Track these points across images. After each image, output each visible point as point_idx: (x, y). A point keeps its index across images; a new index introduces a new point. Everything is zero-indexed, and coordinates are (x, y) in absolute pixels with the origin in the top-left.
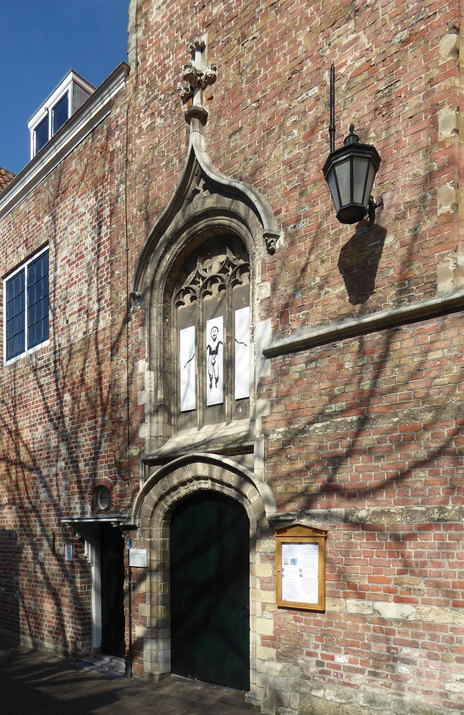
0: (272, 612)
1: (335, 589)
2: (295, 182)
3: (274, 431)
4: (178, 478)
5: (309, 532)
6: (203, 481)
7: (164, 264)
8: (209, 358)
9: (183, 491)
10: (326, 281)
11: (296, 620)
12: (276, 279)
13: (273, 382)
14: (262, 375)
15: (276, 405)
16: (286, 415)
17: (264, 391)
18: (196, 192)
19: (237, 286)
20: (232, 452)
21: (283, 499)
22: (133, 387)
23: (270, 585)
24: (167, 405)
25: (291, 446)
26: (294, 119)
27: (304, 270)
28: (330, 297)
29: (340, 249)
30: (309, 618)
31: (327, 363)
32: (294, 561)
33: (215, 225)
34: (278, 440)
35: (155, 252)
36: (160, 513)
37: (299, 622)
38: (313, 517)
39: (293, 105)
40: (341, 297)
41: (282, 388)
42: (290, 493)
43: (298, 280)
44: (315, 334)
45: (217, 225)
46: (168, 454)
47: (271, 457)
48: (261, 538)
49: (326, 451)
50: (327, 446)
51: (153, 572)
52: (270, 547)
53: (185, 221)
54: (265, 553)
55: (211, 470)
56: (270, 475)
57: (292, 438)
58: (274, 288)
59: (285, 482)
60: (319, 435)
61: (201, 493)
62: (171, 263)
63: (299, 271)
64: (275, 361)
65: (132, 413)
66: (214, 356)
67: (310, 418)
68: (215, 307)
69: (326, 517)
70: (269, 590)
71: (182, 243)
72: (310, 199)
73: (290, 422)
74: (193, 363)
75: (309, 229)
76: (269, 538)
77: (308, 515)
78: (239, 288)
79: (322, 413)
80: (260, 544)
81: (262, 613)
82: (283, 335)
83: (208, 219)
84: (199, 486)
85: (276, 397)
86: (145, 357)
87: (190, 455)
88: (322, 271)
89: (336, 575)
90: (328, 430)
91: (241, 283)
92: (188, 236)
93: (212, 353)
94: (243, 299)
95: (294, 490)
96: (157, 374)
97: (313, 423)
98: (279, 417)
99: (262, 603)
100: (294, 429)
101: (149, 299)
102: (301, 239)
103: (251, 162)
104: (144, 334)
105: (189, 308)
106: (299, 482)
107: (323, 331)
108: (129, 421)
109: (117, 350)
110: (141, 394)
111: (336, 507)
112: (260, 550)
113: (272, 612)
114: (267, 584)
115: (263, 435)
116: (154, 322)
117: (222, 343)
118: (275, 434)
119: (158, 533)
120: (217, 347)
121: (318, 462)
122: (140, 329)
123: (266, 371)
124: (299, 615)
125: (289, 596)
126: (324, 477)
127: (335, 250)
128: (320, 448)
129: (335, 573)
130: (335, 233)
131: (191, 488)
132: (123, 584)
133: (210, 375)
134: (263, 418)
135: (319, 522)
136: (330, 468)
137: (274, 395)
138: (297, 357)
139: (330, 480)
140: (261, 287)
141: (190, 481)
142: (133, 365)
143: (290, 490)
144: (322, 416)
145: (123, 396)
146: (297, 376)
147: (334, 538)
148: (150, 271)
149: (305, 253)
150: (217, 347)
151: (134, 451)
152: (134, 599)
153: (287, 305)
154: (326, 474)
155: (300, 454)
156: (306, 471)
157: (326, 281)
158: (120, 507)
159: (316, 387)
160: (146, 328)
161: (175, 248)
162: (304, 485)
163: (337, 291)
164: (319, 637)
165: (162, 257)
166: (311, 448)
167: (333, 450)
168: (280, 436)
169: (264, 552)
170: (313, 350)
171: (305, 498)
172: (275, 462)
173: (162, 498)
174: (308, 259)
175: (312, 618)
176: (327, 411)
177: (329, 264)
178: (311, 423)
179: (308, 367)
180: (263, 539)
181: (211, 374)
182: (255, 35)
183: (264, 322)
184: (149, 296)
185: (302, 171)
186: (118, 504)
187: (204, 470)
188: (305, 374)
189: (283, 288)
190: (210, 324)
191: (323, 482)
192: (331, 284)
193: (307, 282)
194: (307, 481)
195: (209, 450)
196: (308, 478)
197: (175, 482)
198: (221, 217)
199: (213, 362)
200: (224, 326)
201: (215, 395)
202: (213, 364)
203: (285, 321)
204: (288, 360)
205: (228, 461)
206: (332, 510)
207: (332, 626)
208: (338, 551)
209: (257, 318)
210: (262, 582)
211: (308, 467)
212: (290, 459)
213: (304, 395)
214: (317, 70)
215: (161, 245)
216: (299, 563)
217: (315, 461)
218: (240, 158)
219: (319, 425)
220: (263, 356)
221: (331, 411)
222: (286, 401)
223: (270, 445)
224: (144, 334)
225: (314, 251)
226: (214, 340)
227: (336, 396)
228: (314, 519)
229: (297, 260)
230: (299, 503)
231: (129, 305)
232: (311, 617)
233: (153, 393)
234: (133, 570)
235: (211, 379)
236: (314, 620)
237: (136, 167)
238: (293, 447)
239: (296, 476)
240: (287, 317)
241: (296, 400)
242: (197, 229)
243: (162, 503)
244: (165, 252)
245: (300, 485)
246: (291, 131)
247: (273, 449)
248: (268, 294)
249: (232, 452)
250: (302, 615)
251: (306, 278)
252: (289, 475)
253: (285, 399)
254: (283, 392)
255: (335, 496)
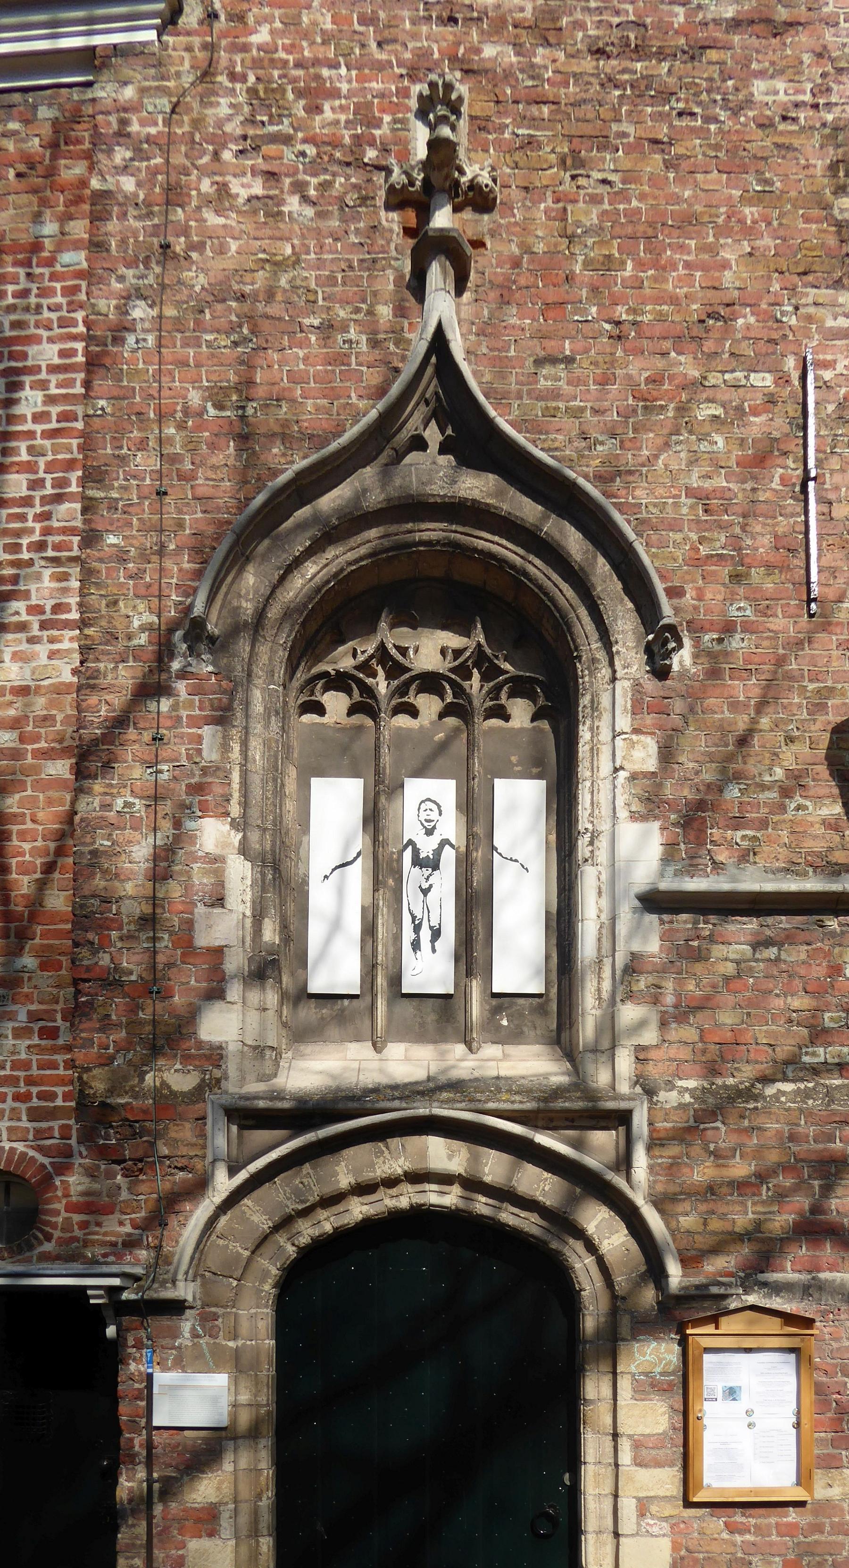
0: (665, 1519)
1: (831, 1450)
2: (718, 544)
3: (670, 1086)
4: (355, 1171)
5: (774, 1325)
6: (434, 1187)
7: (299, 584)
8: (412, 876)
9: (358, 1210)
10: (795, 784)
11: (731, 1528)
12: (671, 737)
13: (662, 970)
14: (636, 947)
15: (674, 1025)
16: (704, 1052)
17: (642, 985)
18: (419, 443)
19: (495, 722)
20: (551, 1120)
21: (696, 1246)
22: (174, 890)
23: (661, 1452)
24: (277, 964)
25: (718, 1124)
26: (717, 413)
27: (743, 741)
28: (810, 819)
29: (830, 728)
30: (766, 1521)
31: (803, 956)
32: (732, 1393)
33: (475, 550)
34: (682, 1106)
35: (278, 537)
36: (270, 1268)
37: (741, 1533)
38: (777, 1289)
39: (712, 381)
40: (830, 825)
41: (691, 987)
42: (714, 1233)
43: (730, 758)
44: (769, 886)
45: (481, 552)
46: (323, 1099)
47: (662, 1145)
48: (634, 1338)
49: (805, 1146)
50: (807, 1136)
51: (240, 1442)
52: (661, 1360)
53: (389, 500)
54: (646, 1374)
55: (475, 1159)
56: (660, 1188)
57: (712, 1109)
58: (667, 754)
59: (703, 1207)
60: (788, 1110)
61: (421, 1216)
62: (318, 590)
63: (731, 739)
64: (671, 922)
65: (170, 965)
66: (427, 872)
67: (764, 1068)
68: (427, 750)
69: (807, 1290)
70: (658, 1464)
71: (363, 551)
72: (758, 596)
73: (712, 1070)
74: (356, 877)
75: (756, 659)
76: (656, 1339)
77: (765, 1284)
78: (501, 729)
79: (793, 1061)
80: (631, 1354)
81: (638, 1524)
82: (691, 868)
83: (454, 527)
84: (418, 1199)
85: (676, 1006)
86: (227, 814)
87: (422, 1111)
88: (789, 757)
89: (831, 1419)
90: (810, 1102)
91: (507, 718)
92: (386, 543)
93: (417, 862)
94: (514, 759)
95: (726, 1226)
96: (263, 875)
97: (773, 1081)
98: (684, 1053)
99: (639, 1499)
100: (726, 1087)
101: (246, 656)
102: (737, 674)
103: (599, 448)
104: (225, 748)
105: (339, 728)
106: (738, 1208)
107: (792, 885)
108: (154, 986)
109: (108, 766)
110: (208, 916)
111: (831, 1270)
112: (633, 1369)
113: (665, 1519)
114: (654, 1452)
115: (638, 1090)
116: (257, 728)
117: (452, 846)
118: (674, 1093)
119: (255, 1323)
120: (438, 852)
121: (786, 1168)
122: (207, 731)
123: (645, 940)
124: (738, 1517)
125: (719, 1476)
126: (802, 1202)
127: (819, 725)
128: (792, 1138)
129: (829, 1415)
130: (819, 691)
131: (390, 1203)
132: (116, 1482)
133: (414, 918)
134: (640, 1049)
135: (790, 1301)
136: (816, 1183)
137: (670, 1000)
138: (731, 927)
139: (816, 1209)
140: (632, 744)
141: (391, 1182)
142: (177, 824)
143: (715, 1225)
144: (789, 1067)
145: (132, 909)
146: (730, 968)
147: (827, 1337)
148: (251, 581)
149: (746, 706)
150: (438, 852)
151: (179, 1079)
152: (166, 1530)
153: (701, 805)
154: (807, 1196)
155: (741, 1145)
156: (758, 1186)
157: (795, 784)
158: (86, 1244)
159: (779, 1003)
160: (235, 733)
161: (338, 557)
162: (751, 1216)
163: (825, 812)
164: (792, 1561)
165: (297, 563)
166: (768, 1134)
167: (821, 1146)
168: (687, 1098)
169: (641, 1374)
170: (770, 920)
171: (756, 1246)
172: (673, 1158)
173: (285, 1223)
174: (754, 721)
175: (773, 1520)
176: (806, 1059)
177: (802, 749)
178: (766, 1080)
179: (757, 956)
180: (638, 1341)
181: (419, 916)
182: (612, 177)
183: (637, 827)
184: (248, 649)
185: (737, 530)
186: (78, 1233)
187: (450, 1157)
188: (751, 969)
189: (691, 765)
190: (416, 789)
191: (801, 1213)
192: (811, 793)
193: (752, 768)
194: (760, 1209)
195: (491, 1105)
196: (763, 1203)
197: (345, 1181)
198: (496, 538)
199: (425, 886)
200: (458, 807)
201: (429, 970)
202: (425, 892)
203: (697, 838)
204: (706, 929)
205: (544, 1139)
206: (823, 1276)
207: (822, 1532)
208: (836, 1366)
209: (623, 814)
210: (637, 1445)
211: (762, 1177)
212: (716, 1154)
213: (749, 1014)
214: (769, 341)
215: (301, 526)
216: (744, 1396)
217: (779, 1164)
218: (571, 425)
219: (788, 1087)
220: (637, 903)
221: (816, 1060)
222: (700, 1018)
223: (660, 1115)
224: (225, 748)
225: (770, 709)
226: (429, 832)
227: (826, 1031)
228: (777, 1295)
229: (727, 714)
230: (740, 1258)
231: (164, 651)
232: (772, 1518)
233: (248, 922)
234: (157, 1438)
235: (417, 928)
236: (777, 1524)
237: (202, 280)
238: (723, 1129)
239: (732, 1195)
240: (702, 831)
241: (729, 1021)
242: (417, 536)
243: (281, 1239)
244: (310, 553)
245: (742, 1215)
246: (709, 434)
247: (669, 1125)
248: (651, 764)
249: (551, 1120)
250: (750, 1516)
251: (751, 761)
252: (711, 1190)
253: (700, 1016)
254: (693, 998)
255: (828, 1246)
